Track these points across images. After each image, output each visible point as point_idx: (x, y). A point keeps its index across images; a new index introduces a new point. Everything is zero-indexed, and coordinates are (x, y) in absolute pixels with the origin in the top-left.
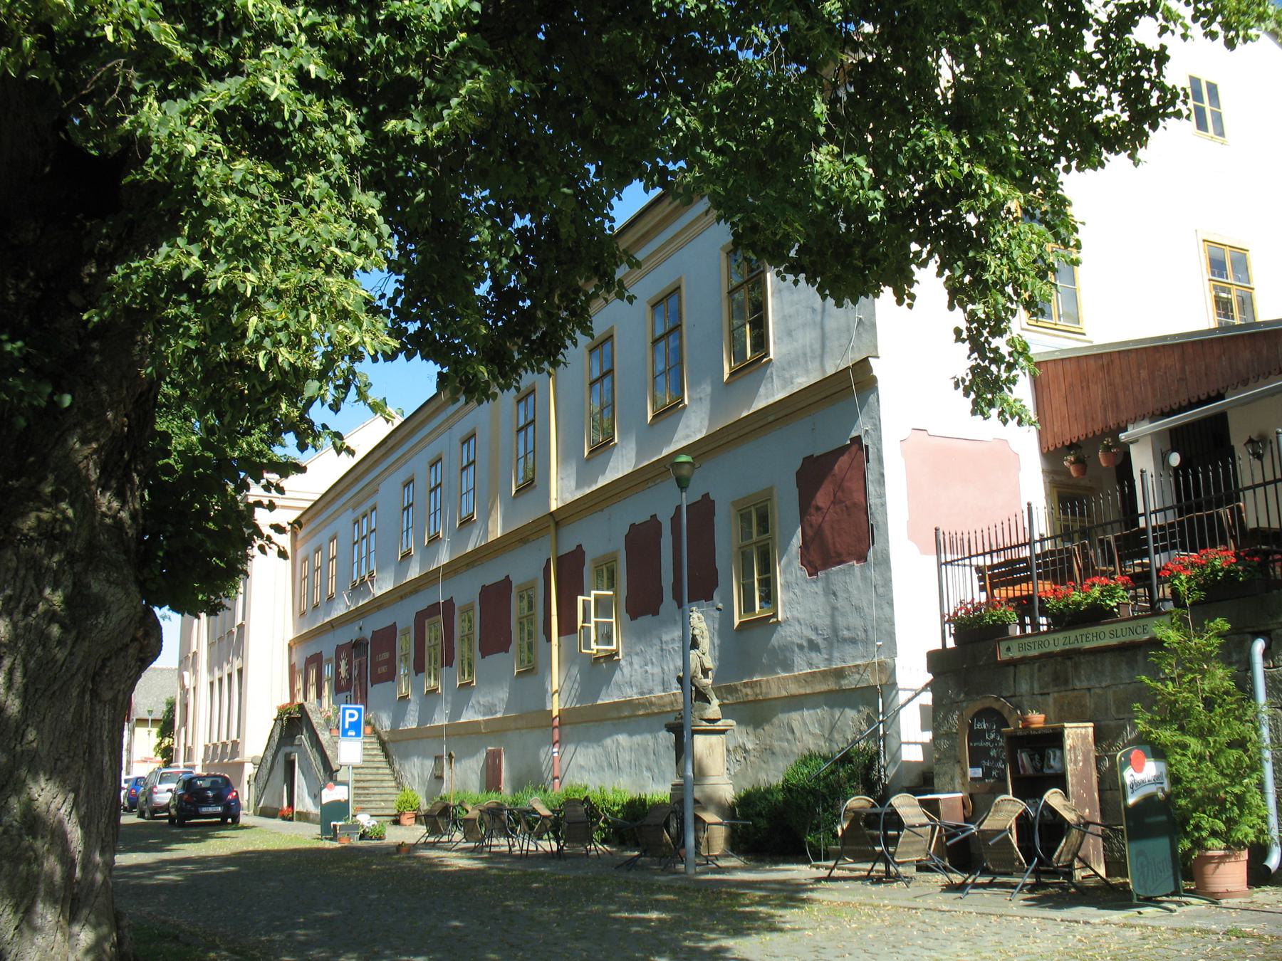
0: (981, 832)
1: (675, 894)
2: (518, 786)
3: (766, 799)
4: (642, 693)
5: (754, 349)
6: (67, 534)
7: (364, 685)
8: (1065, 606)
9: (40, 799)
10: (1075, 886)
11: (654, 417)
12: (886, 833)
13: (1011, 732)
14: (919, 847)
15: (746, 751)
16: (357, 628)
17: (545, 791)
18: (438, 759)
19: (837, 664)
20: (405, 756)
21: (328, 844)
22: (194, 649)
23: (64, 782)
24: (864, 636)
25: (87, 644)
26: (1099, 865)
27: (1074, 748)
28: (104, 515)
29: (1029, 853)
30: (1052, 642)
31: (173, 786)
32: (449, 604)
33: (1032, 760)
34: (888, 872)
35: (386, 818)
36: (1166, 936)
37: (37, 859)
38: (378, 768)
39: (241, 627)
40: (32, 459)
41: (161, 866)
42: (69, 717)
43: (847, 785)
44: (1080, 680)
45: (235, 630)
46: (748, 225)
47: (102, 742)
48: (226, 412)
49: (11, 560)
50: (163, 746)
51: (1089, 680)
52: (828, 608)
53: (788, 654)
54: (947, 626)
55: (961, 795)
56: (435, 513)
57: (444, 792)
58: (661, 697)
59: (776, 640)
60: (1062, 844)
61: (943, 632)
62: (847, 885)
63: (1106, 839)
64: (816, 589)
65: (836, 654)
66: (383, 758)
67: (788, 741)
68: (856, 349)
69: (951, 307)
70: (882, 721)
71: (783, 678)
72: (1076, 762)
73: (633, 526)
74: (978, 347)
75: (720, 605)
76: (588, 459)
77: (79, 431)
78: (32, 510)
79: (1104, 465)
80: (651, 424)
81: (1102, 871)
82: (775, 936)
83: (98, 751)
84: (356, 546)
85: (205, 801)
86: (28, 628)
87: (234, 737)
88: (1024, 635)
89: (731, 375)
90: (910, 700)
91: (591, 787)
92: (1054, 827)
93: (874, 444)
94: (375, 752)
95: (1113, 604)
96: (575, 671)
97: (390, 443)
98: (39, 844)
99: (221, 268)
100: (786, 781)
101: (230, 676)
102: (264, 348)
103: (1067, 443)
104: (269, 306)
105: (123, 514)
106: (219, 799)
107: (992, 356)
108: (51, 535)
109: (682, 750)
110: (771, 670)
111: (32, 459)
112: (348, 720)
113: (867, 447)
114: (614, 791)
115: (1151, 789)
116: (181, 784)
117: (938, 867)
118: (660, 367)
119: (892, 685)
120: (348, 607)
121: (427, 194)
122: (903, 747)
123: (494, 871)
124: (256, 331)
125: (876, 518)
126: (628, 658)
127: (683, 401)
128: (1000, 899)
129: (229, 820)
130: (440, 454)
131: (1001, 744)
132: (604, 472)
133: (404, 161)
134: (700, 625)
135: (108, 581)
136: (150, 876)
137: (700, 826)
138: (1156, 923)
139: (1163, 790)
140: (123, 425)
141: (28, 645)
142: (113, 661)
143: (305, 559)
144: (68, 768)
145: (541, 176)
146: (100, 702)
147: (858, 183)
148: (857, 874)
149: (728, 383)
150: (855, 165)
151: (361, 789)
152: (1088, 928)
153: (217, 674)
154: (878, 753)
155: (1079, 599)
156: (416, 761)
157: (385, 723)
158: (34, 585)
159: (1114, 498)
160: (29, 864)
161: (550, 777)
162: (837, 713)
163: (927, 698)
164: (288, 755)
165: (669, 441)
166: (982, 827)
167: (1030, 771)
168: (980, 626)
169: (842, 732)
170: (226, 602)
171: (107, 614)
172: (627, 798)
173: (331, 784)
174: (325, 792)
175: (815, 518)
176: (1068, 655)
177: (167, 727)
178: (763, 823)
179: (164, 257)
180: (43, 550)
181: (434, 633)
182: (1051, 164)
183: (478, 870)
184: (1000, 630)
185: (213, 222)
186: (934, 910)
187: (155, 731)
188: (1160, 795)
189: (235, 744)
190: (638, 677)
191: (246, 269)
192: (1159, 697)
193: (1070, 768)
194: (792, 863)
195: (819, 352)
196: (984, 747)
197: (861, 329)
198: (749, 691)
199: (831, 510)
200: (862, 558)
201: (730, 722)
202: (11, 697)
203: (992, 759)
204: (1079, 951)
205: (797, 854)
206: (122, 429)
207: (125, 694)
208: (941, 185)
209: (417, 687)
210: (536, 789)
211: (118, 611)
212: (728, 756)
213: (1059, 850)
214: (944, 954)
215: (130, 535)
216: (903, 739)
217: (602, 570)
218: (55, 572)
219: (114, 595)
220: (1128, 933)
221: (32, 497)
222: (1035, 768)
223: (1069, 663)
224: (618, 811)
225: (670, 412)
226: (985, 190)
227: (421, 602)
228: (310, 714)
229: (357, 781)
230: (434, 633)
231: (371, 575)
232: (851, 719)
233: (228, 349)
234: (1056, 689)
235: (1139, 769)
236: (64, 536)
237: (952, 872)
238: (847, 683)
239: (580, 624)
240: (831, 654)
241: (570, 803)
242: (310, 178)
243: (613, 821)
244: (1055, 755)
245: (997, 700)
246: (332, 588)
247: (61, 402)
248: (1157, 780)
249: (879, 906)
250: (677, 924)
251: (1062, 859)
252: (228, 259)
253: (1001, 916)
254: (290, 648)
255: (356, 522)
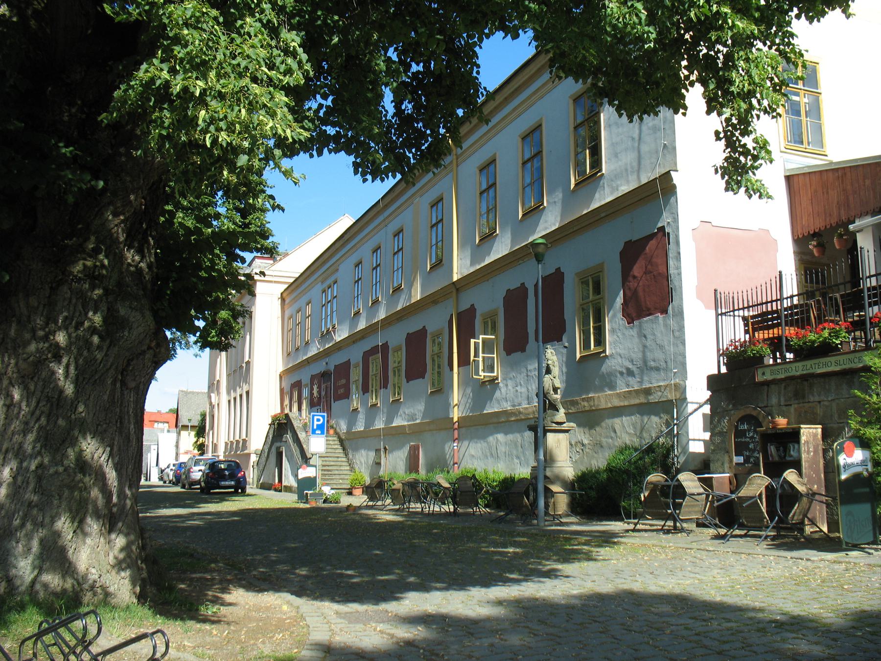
0: (739, 498)
1: (528, 538)
2: (430, 469)
3: (595, 477)
4: (514, 406)
5: (592, 167)
6: (103, 276)
7: (329, 404)
8: (804, 343)
9: (88, 450)
10: (804, 537)
11: (523, 215)
12: (674, 501)
13: (764, 431)
14: (697, 509)
15: (583, 445)
16: (324, 363)
17: (448, 472)
18: (378, 451)
19: (646, 385)
20: (356, 449)
21: (302, 506)
22: (218, 378)
23: (103, 440)
24: (665, 366)
25: (116, 349)
26: (823, 524)
27: (807, 442)
28: (129, 265)
29: (772, 513)
30: (794, 368)
31: (203, 468)
32: (385, 346)
33: (778, 450)
34: (675, 527)
35: (343, 491)
36: (862, 569)
37: (86, 489)
38: (338, 457)
39: (248, 363)
40: (80, 226)
41: (191, 516)
42: (106, 397)
43: (650, 468)
44: (813, 395)
45: (244, 365)
46: (558, 51)
47: (129, 416)
48: (192, 180)
49: (66, 293)
50: (198, 443)
51: (819, 395)
52: (641, 346)
53: (613, 378)
54: (721, 358)
55: (728, 475)
56: (376, 284)
57: (381, 473)
58: (527, 408)
59: (604, 369)
60: (795, 508)
61: (719, 362)
62: (646, 534)
63: (828, 505)
64: (632, 333)
65: (646, 378)
66: (341, 451)
67: (612, 438)
68: (662, 166)
69: (708, 113)
70: (676, 424)
71: (609, 395)
72: (808, 452)
73: (508, 291)
74: (731, 144)
75: (566, 344)
76: (479, 245)
77: (111, 208)
78: (79, 260)
79: (837, 247)
80: (522, 220)
81: (825, 529)
82: (591, 563)
83: (126, 421)
84: (324, 308)
85: (224, 478)
86: (78, 338)
87: (244, 437)
88: (776, 364)
89: (576, 185)
90: (696, 410)
91: (479, 470)
92: (791, 496)
93: (674, 232)
94: (336, 447)
95: (837, 342)
96: (469, 390)
97: (346, 237)
98: (87, 479)
99: (179, 77)
100: (609, 464)
101: (241, 396)
102: (210, 132)
103: (812, 232)
104: (214, 104)
105: (142, 264)
106: (232, 476)
107: (741, 150)
108: (93, 276)
109: (538, 443)
110: (601, 389)
111: (80, 226)
112: (316, 423)
113: (668, 234)
114: (494, 472)
115: (859, 469)
116: (208, 466)
117: (710, 524)
118: (528, 180)
119: (683, 400)
120: (319, 349)
121: (339, 38)
122: (690, 442)
123: (410, 523)
124: (204, 121)
125: (674, 283)
126: (505, 382)
127: (543, 204)
128: (752, 544)
129: (240, 491)
130: (380, 244)
131: (757, 440)
132: (489, 254)
133: (322, 14)
134: (552, 358)
135: (130, 307)
136: (183, 522)
137: (549, 495)
138: (857, 561)
139: (867, 470)
140: (141, 205)
141: (78, 349)
142: (134, 362)
143: (290, 317)
144: (105, 431)
145: (422, 27)
146: (127, 389)
147: (637, 21)
148: (655, 528)
149: (574, 191)
150: (636, 8)
151: (326, 471)
152: (809, 563)
153: (233, 395)
154: (673, 446)
155: (814, 338)
156: (363, 452)
157: (343, 427)
158: (82, 309)
159: (841, 267)
160: (81, 491)
161: (452, 463)
162: (646, 419)
163: (707, 409)
164: (278, 448)
165: (534, 232)
166: (739, 495)
167: (777, 459)
168: (744, 357)
169: (649, 432)
170: (233, 342)
171: (130, 329)
172: (502, 477)
173: (305, 465)
174: (300, 471)
175: (633, 284)
176: (805, 378)
177: (201, 431)
178: (593, 494)
179: (143, 73)
180: (87, 286)
181: (375, 368)
182: (786, 12)
183: (399, 522)
184: (758, 360)
185: (177, 48)
186: (703, 550)
187: (193, 433)
188: (865, 473)
189: (244, 441)
190: (511, 395)
191: (197, 78)
192: (867, 406)
193: (804, 456)
194: (612, 521)
195: (636, 168)
196: (745, 442)
197: (666, 151)
198: (586, 404)
199: (643, 278)
200: (665, 311)
201: (572, 424)
202: (68, 383)
203: (750, 450)
204: (798, 577)
205: (615, 515)
206: (141, 207)
207: (144, 385)
208: (695, 19)
209: (364, 403)
210: (442, 471)
211: (138, 327)
212: (570, 448)
213: (793, 512)
214: (705, 576)
215: (147, 279)
216: (690, 437)
217: (488, 321)
218: (96, 301)
219: (134, 317)
220: (836, 566)
221: (79, 251)
222: (779, 456)
223: (806, 383)
224: (496, 486)
225: (534, 211)
226: (728, 24)
227: (366, 345)
228: (292, 420)
229: (323, 466)
230: (375, 368)
231: (333, 327)
232: (655, 423)
233: (186, 134)
234: (797, 401)
235: (850, 455)
236: (101, 277)
237: (721, 527)
238: (653, 398)
239: (472, 358)
240: (642, 378)
241: (463, 478)
242: (248, 20)
243: (493, 492)
244: (794, 448)
245: (755, 409)
246: (308, 337)
247: (97, 186)
248: (863, 463)
249: (666, 547)
250: (524, 556)
251: (795, 518)
252: (185, 71)
253: (749, 554)
254: (281, 377)
255: (324, 291)
